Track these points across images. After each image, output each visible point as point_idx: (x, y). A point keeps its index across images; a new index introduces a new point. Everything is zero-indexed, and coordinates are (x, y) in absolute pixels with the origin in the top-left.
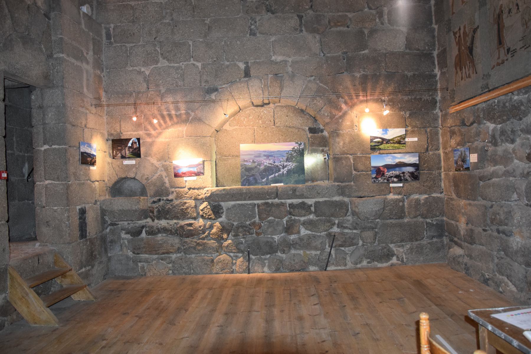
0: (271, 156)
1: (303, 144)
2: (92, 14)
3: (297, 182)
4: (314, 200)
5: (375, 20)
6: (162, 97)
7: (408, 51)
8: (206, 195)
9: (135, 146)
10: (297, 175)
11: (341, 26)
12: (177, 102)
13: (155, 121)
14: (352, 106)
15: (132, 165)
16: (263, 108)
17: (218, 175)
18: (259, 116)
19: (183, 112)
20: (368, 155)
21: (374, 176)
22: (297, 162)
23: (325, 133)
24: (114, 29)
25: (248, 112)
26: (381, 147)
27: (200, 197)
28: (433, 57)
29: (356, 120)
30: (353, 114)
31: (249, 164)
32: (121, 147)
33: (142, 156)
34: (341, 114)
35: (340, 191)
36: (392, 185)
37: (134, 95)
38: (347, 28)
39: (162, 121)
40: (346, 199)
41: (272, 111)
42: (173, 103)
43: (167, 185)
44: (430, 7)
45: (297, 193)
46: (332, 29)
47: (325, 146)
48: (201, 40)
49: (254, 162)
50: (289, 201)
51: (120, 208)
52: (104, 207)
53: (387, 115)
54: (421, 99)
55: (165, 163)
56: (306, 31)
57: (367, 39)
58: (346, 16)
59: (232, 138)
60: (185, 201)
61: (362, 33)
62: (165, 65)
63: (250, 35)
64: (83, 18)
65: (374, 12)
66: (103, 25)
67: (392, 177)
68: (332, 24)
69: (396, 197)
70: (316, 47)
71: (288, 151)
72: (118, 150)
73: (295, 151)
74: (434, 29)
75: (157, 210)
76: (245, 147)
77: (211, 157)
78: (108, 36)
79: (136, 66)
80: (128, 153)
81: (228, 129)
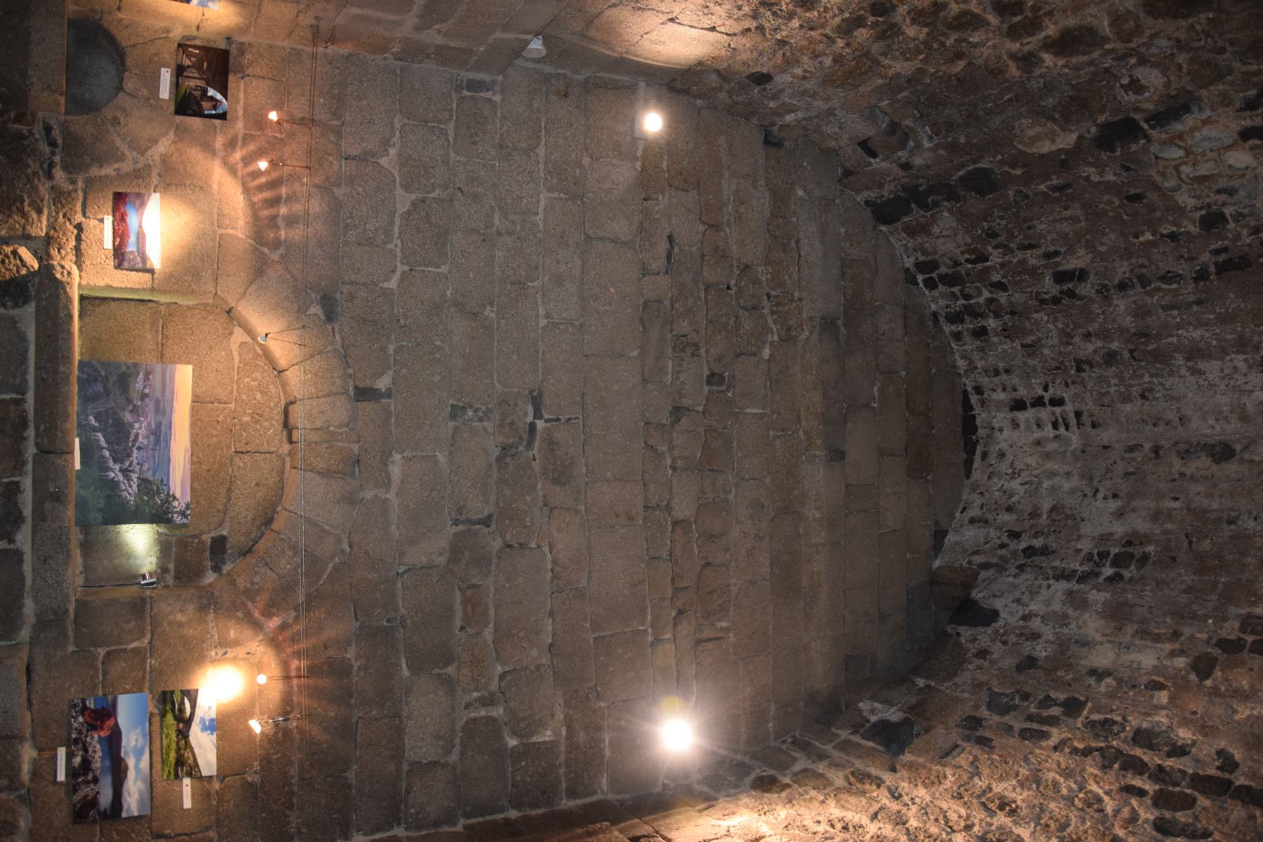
0: (157, 441)
1: (185, 521)
2: (527, 60)
3: (82, 504)
4: (27, 548)
5: (476, 690)
6: (324, 189)
7: (405, 767)
8: (59, 268)
9: (204, 104)
10: (102, 503)
11: (465, 614)
12: (307, 224)
13: (263, 165)
14: (274, 642)
16: (280, 428)
17: (113, 304)
18: (261, 416)
19: (283, 234)
20: (147, 685)
21: (91, 704)
22: (137, 506)
23: (210, 577)
24: (490, 100)
25: (273, 391)
26: (170, 717)
27: (54, 252)
28: (391, 827)
29: (241, 651)
30: (257, 647)
31: (138, 384)
33: (179, 118)
34: (257, 615)
35: (51, 616)
36: (62, 752)
37: (335, 123)
38: (459, 626)
39: (263, 180)
40: (25, 634)
41: (272, 449)
42: (307, 212)
43: (95, 171)
44: (502, 810)
45: (48, 506)
46: (458, 593)
47: (177, 577)
48: (448, 293)
49: (144, 396)
50: (27, 483)
53: (250, 729)
54: (291, 807)
55: (154, 174)
56: (455, 534)
57: (434, 672)
58: (487, 625)
59: (211, 348)
60: (46, 212)
61: (448, 663)
62: (398, 206)
63: (452, 406)
64: (516, 39)
65: (494, 686)
66: (500, 77)
67: (85, 750)
68: (469, 593)
69: (26, 768)
70: (418, 555)
71: (168, 485)
72: (200, 61)
73: (167, 501)
74: (454, 824)
75: (25, 132)
76: (184, 377)
77: (163, 292)
78: (475, 86)
79: (401, 137)
80: (192, 83)
81: (233, 339)
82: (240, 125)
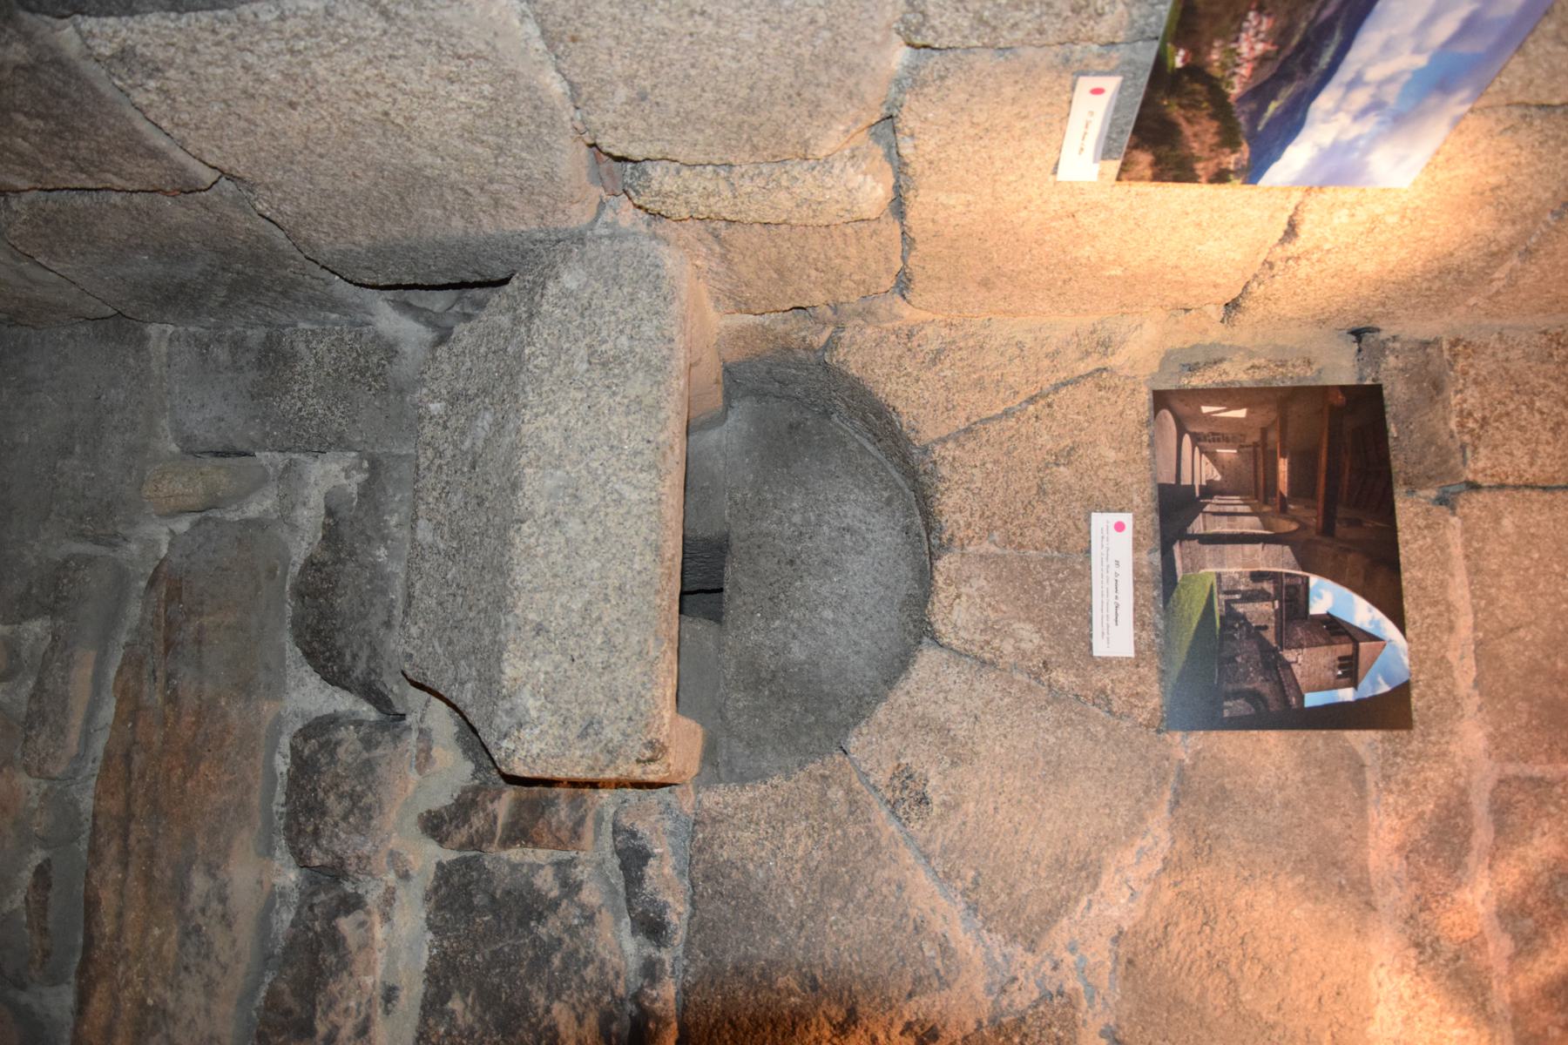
9: (1308, 663)
15: (1084, 612)
32: (1302, 486)
33: (1185, 746)
51: (538, 487)
52: (571, 279)
72: (1261, 456)
75: (546, 882)
82: (1471, 739)
